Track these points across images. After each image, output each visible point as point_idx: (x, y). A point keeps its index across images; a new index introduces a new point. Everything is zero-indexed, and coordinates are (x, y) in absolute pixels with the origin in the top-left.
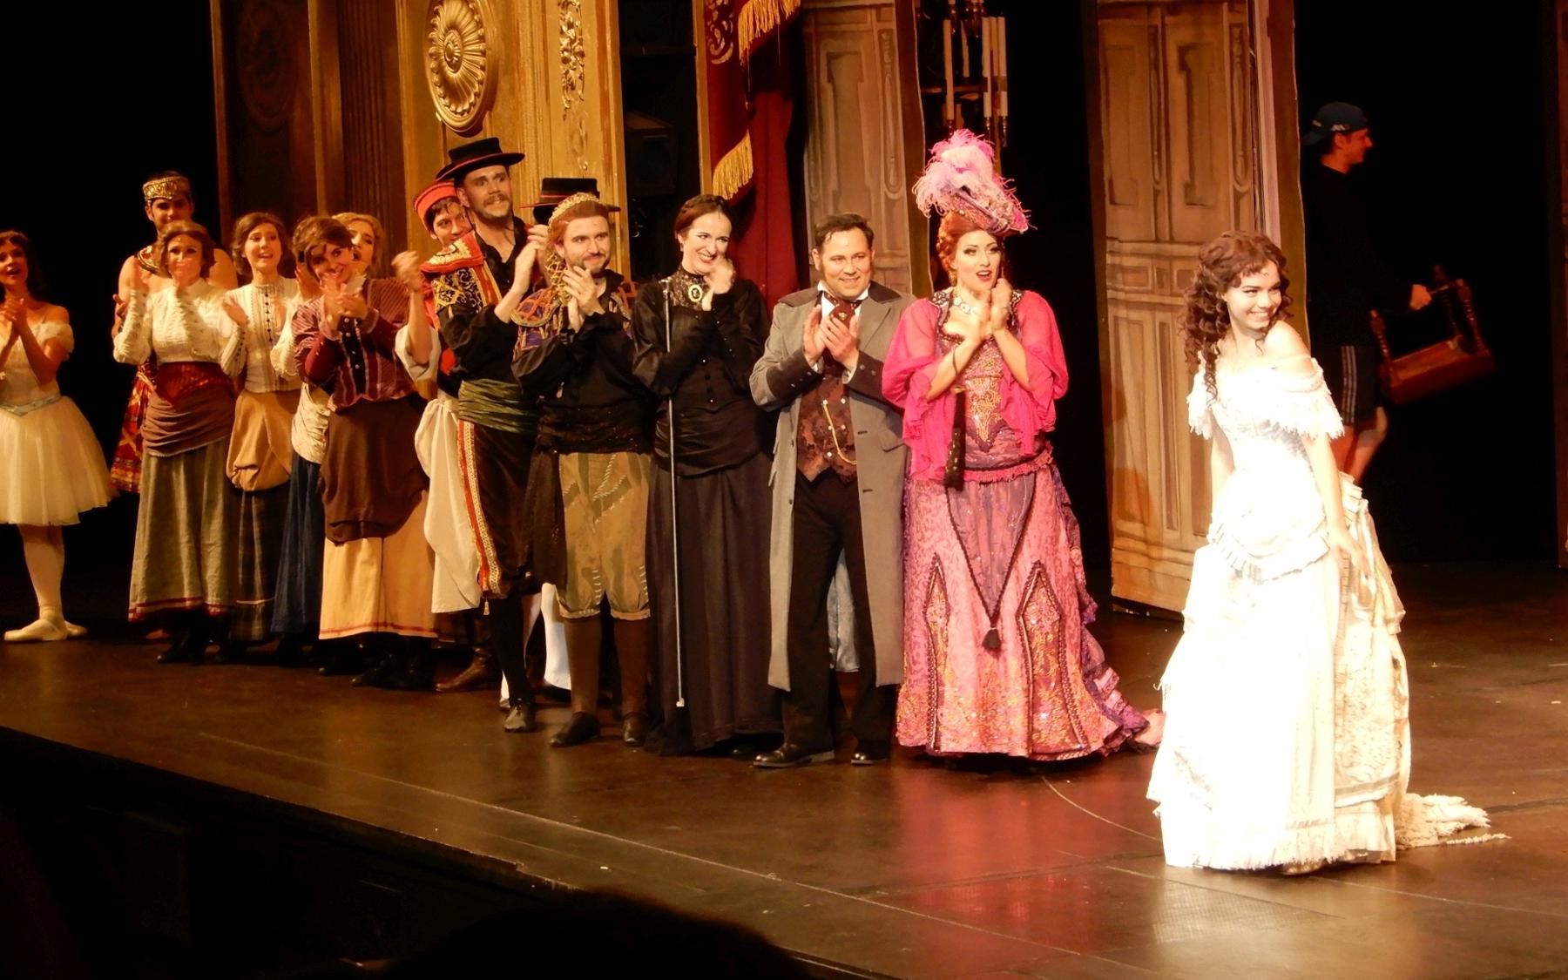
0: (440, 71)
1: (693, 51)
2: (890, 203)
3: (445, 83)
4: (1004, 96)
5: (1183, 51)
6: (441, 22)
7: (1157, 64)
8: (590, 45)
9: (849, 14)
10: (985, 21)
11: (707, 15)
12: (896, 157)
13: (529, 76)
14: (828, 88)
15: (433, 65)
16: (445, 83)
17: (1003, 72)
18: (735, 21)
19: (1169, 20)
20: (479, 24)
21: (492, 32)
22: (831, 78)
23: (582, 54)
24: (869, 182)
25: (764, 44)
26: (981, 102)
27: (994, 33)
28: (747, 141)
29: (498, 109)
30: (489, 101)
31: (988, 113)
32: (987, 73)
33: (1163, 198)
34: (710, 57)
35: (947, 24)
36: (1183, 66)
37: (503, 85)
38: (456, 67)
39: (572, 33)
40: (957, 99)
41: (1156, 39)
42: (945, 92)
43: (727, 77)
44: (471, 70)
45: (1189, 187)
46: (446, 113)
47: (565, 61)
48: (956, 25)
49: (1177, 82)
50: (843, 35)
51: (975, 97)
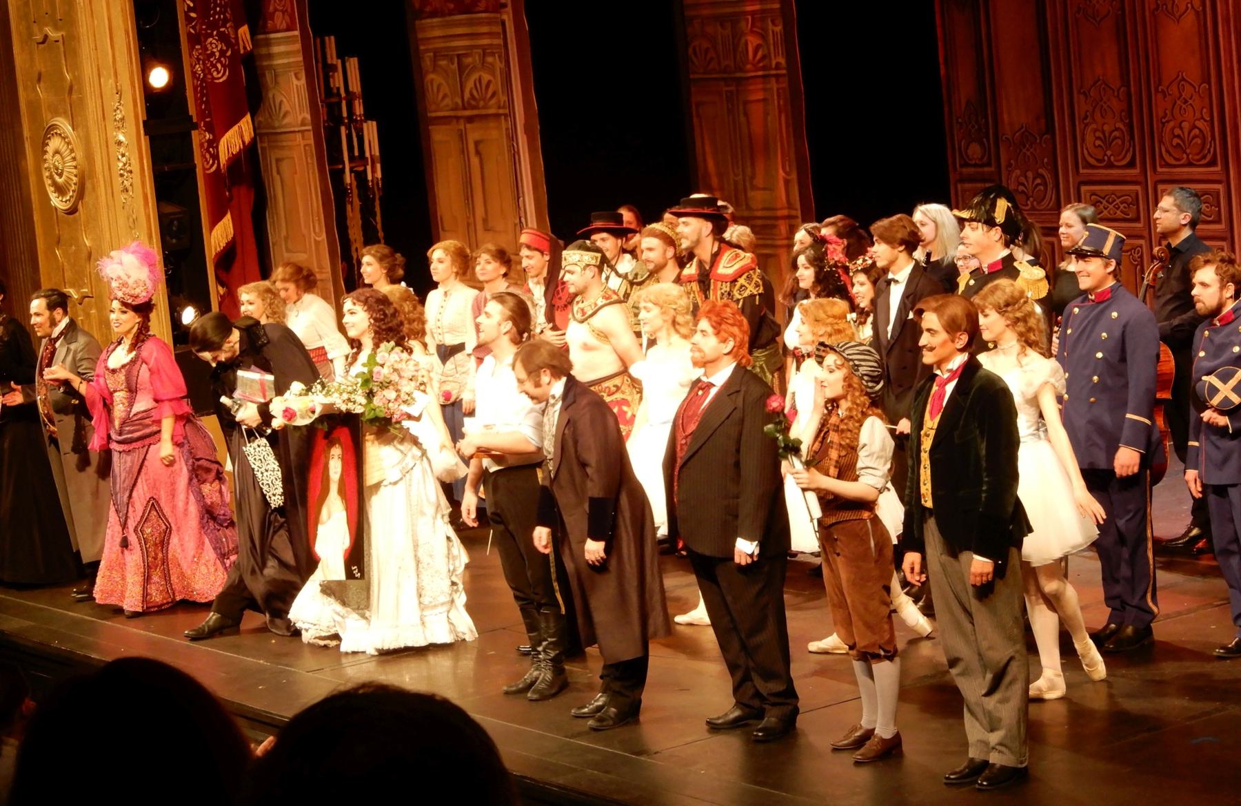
0: (51, 177)
1: (195, 166)
2: (317, 243)
3: (55, 184)
4: (378, 166)
5: (477, 143)
6: (50, 149)
7: (464, 151)
8: (135, 167)
9: (283, 136)
10: (365, 125)
11: (202, 145)
12: (318, 215)
13: (102, 182)
14: (277, 178)
15: (47, 174)
16: (55, 184)
17: (377, 152)
18: (217, 147)
19: (468, 126)
20: (72, 151)
21: (79, 154)
22: (278, 172)
23: (131, 172)
24: (305, 231)
25: (234, 161)
26: (365, 171)
27: (371, 131)
28: (229, 216)
29: (86, 199)
30: (81, 194)
31: (370, 178)
32: (367, 154)
33: (472, 227)
34: (204, 169)
35: (343, 129)
36: (478, 153)
37: (88, 185)
38: (60, 175)
39: (124, 159)
40: (351, 171)
41: (462, 137)
42: (344, 168)
43: (215, 180)
44: (69, 175)
45: (485, 221)
46: (56, 201)
47: (122, 175)
48: (349, 128)
49: (475, 161)
50: (282, 148)
51: (362, 169)
